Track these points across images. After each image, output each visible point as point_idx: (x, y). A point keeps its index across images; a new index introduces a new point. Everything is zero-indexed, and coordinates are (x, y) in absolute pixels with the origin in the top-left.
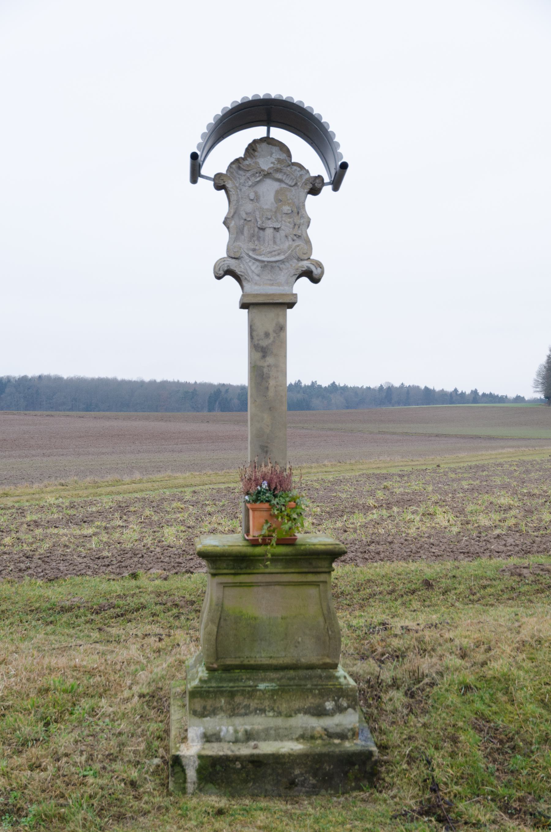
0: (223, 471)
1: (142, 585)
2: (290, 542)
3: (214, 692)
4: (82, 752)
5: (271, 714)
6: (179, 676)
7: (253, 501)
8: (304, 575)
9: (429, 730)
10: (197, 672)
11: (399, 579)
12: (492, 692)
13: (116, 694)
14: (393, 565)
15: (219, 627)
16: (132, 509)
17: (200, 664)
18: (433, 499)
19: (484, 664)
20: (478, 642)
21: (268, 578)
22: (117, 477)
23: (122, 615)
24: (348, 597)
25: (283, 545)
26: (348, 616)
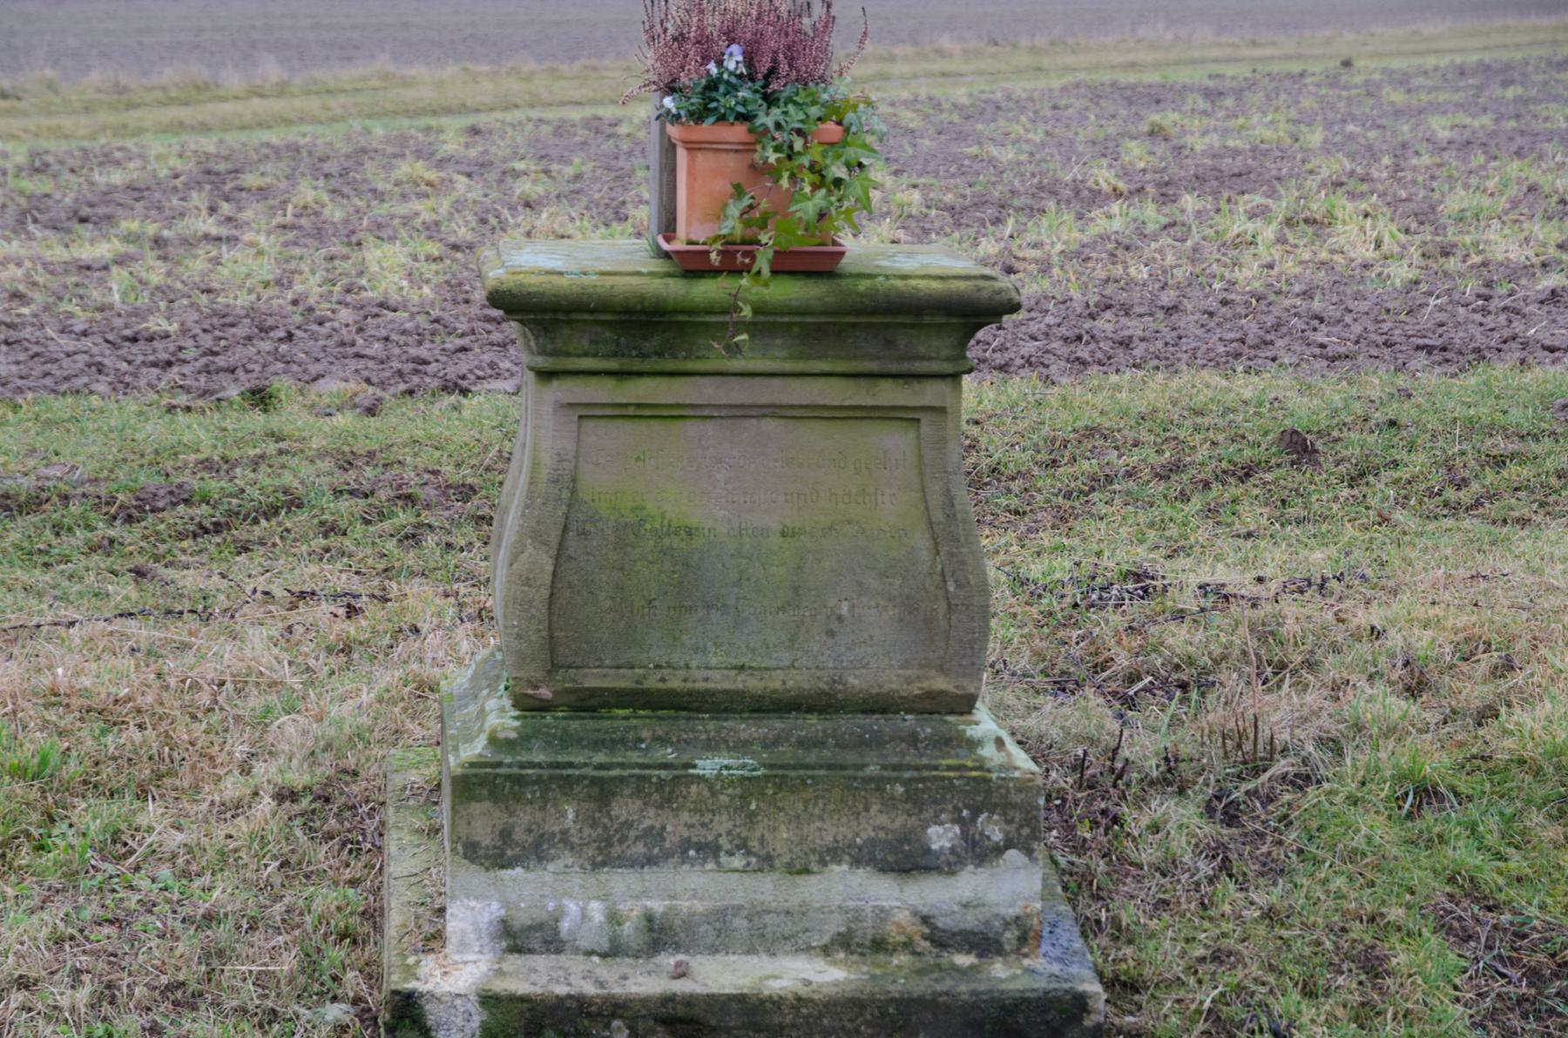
0: (577, 65)
1: (288, 429)
2: (819, 263)
3: (538, 781)
4: (77, 973)
5: (737, 862)
6: (419, 732)
7: (691, 114)
8: (863, 382)
9: (1285, 933)
10: (482, 714)
11: (1197, 429)
12: (1509, 811)
13: (197, 789)
14: (1175, 383)
15: (560, 556)
16: (251, 180)
17: (493, 688)
18: (1325, 173)
19: (1487, 714)
20: (1467, 640)
21: (738, 392)
22: (199, 72)
23: (218, 528)
24: (1016, 486)
25: (793, 273)
26: (1015, 548)
